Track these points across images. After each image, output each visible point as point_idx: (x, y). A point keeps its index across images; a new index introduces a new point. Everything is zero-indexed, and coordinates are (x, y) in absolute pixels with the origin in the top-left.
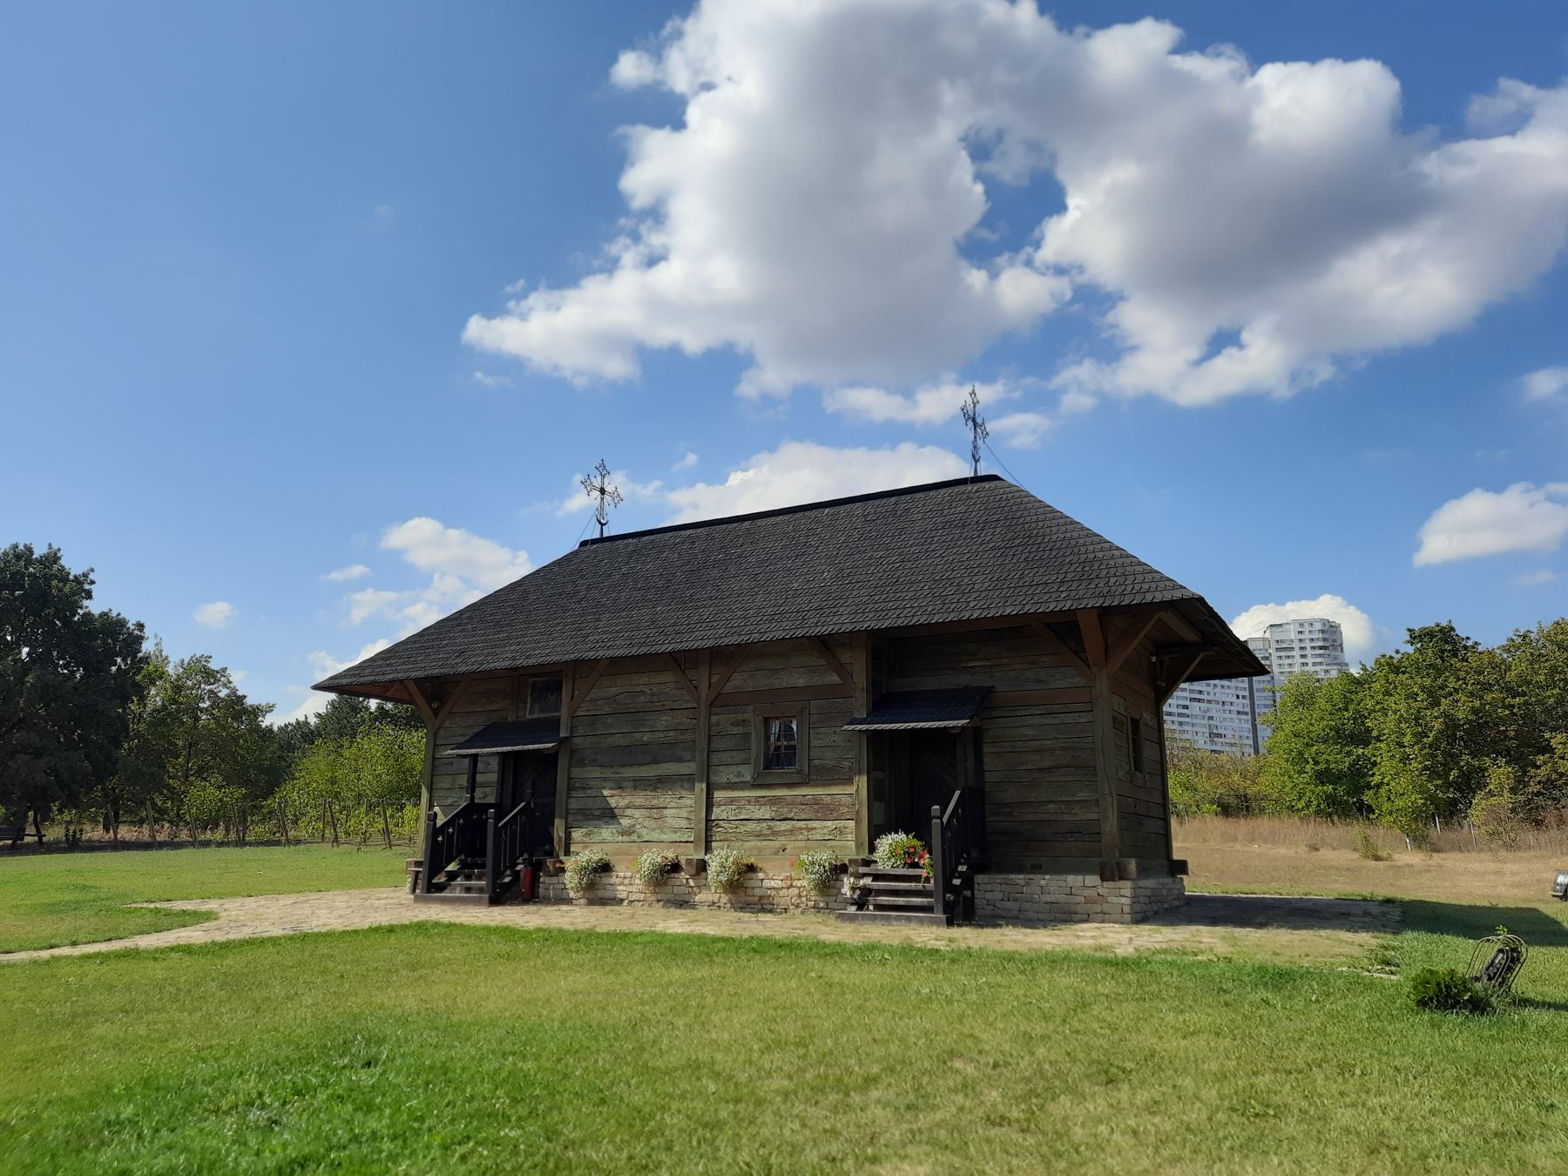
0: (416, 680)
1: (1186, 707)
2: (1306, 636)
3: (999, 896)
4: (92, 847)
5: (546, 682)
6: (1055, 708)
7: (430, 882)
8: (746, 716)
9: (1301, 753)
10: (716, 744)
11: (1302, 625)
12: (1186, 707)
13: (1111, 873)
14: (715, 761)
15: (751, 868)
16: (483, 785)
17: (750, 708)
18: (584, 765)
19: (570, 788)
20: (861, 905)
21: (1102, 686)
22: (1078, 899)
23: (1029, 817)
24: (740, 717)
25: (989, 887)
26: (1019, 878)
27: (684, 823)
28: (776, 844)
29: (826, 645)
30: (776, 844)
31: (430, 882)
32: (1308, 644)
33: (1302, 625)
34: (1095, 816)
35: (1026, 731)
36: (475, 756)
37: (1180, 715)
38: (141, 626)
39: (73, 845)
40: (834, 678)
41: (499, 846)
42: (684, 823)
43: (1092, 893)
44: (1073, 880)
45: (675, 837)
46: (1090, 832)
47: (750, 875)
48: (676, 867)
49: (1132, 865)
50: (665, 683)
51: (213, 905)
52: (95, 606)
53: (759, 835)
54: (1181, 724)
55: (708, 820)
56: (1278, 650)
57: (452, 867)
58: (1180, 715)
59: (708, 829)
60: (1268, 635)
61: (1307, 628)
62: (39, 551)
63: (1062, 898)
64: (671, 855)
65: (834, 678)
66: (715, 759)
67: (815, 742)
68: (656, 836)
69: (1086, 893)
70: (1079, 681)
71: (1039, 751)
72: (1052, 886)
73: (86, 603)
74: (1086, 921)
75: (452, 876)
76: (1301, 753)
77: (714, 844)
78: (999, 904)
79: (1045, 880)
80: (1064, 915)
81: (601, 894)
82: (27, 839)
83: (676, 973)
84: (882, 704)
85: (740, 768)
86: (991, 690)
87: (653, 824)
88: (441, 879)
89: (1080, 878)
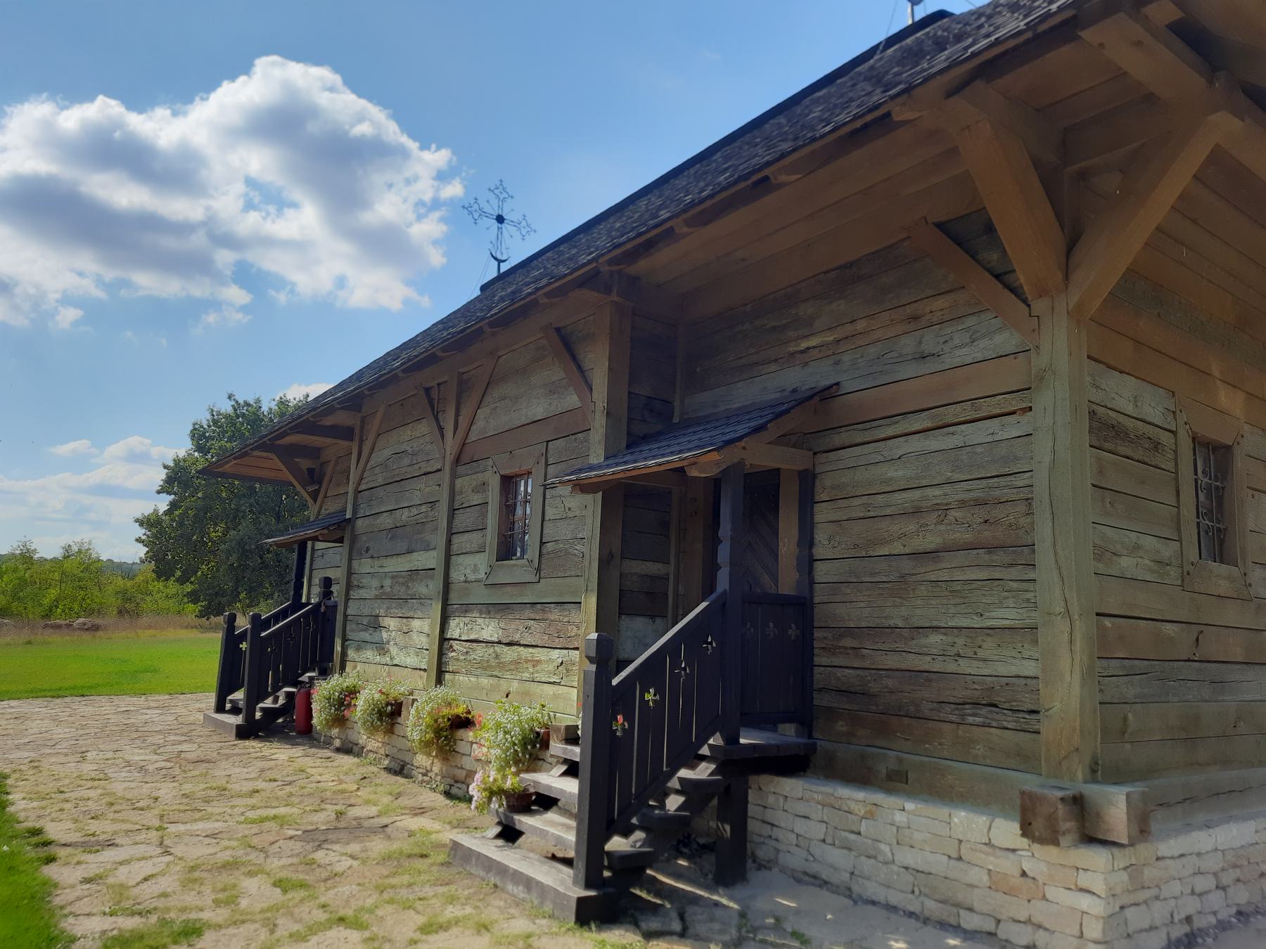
3: (817, 831)
6: (951, 414)
10: (463, 520)
14: (455, 548)
21: (1058, 345)
22: (977, 876)
23: (892, 661)
25: (801, 808)
34: (1029, 668)
43: (1007, 865)
44: (966, 822)
46: (1008, 706)
47: (461, 733)
53: (484, 667)
59: (441, 654)
63: (937, 863)
69: (993, 862)
70: (1006, 340)
77: (447, 676)
78: (818, 850)
79: (903, 812)
83: (301, 876)
84: (643, 420)
86: (827, 394)
89: (982, 820)
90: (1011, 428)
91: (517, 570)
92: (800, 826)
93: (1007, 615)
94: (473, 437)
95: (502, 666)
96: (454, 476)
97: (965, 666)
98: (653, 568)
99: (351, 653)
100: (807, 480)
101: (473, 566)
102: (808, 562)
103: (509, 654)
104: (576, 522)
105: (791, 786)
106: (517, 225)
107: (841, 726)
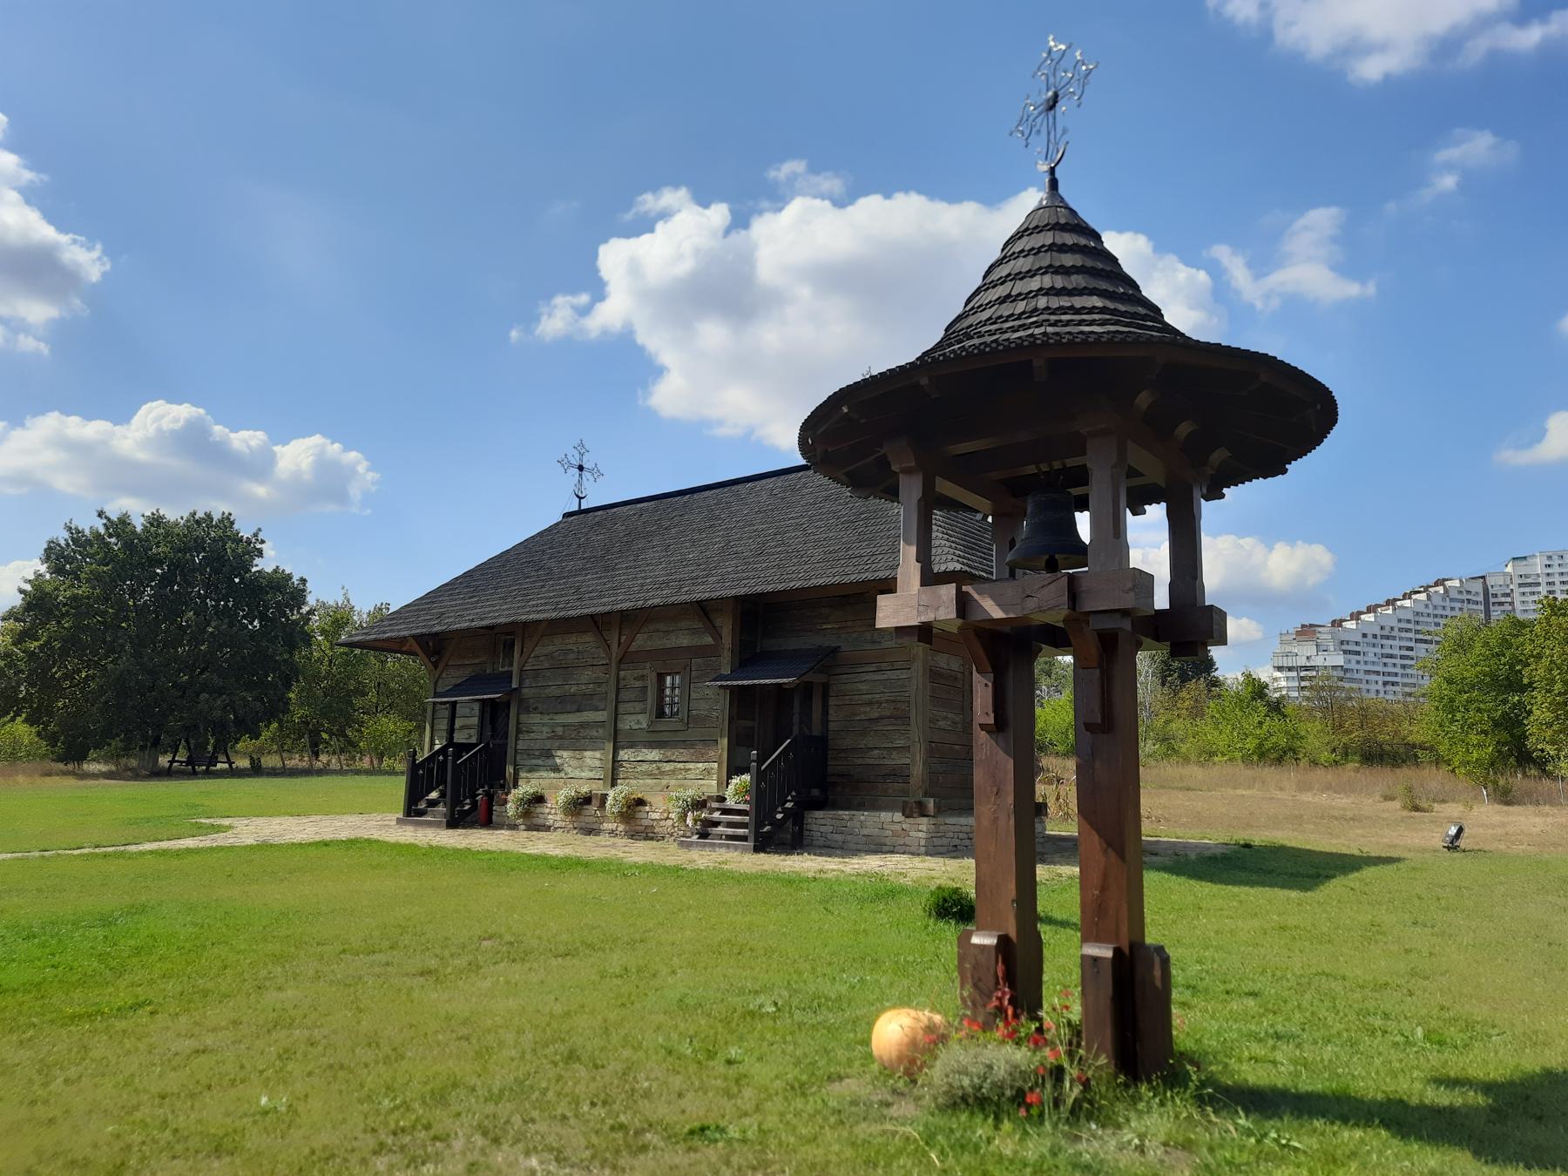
0: (414, 636)
1: (1411, 649)
2: (1556, 569)
4: (274, 773)
5: (503, 638)
7: (413, 809)
8: (645, 672)
9: (1452, 700)
10: (624, 695)
11: (1550, 558)
12: (1411, 649)
13: (915, 810)
15: (641, 802)
16: (463, 728)
17: (648, 665)
18: (529, 712)
19: (519, 731)
20: (704, 835)
23: (859, 761)
24: (640, 672)
26: (845, 814)
27: (598, 763)
28: (664, 782)
29: (704, 610)
30: (664, 782)
31: (413, 809)
32: (1557, 579)
33: (1550, 558)
35: (861, 686)
36: (455, 703)
37: (1402, 657)
38: (303, 581)
39: (256, 770)
40: (708, 640)
41: (465, 785)
42: (598, 763)
43: (898, 827)
44: (885, 816)
45: (591, 775)
46: (901, 774)
48: (587, 800)
49: (931, 804)
50: (586, 642)
51: (226, 822)
52: (265, 564)
53: (650, 775)
54: (1404, 667)
55: (615, 761)
56: (1520, 585)
57: (434, 795)
58: (1402, 657)
59: (614, 769)
60: (1509, 569)
61: (1556, 561)
62: (62, 536)
63: (876, 832)
64: (584, 790)
65: (708, 640)
66: (622, 708)
67: (693, 695)
68: (577, 773)
71: (870, 703)
72: (869, 821)
73: (257, 561)
74: (892, 852)
75: (433, 803)
76: (1452, 700)
79: (863, 816)
80: (877, 847)
81: (536, 821)
82: (219, 766)
84: (747, 659)
85: (640, 717)
86: (836, 650)
87: (574, 763)
88: (422, 805)
90: (904, 675)
91: (662, 725)
92: (823, 829)
93: (900, 743)
94: (632, 649)
95: (662, 773)
96: (619, 670)
97: (886, 762)
98: (749, 723)
99: (523, 774)
100: (825, 688)
101: (636, 721)
102: (825, 721)
103: (668, 767)
104: (711, 699)
105: (818, 814)
106: (590, 471)
107: (839, 789)
